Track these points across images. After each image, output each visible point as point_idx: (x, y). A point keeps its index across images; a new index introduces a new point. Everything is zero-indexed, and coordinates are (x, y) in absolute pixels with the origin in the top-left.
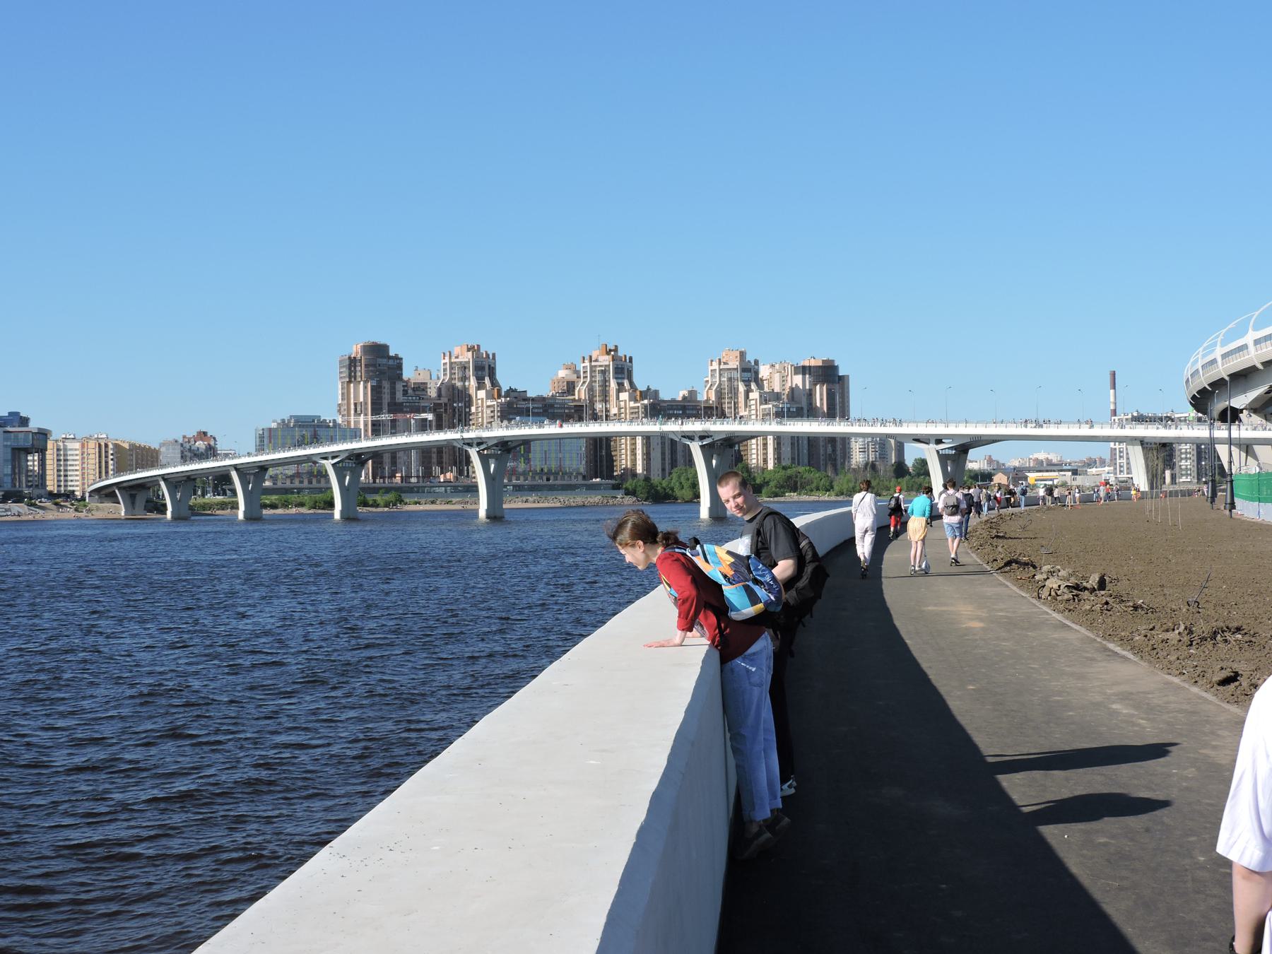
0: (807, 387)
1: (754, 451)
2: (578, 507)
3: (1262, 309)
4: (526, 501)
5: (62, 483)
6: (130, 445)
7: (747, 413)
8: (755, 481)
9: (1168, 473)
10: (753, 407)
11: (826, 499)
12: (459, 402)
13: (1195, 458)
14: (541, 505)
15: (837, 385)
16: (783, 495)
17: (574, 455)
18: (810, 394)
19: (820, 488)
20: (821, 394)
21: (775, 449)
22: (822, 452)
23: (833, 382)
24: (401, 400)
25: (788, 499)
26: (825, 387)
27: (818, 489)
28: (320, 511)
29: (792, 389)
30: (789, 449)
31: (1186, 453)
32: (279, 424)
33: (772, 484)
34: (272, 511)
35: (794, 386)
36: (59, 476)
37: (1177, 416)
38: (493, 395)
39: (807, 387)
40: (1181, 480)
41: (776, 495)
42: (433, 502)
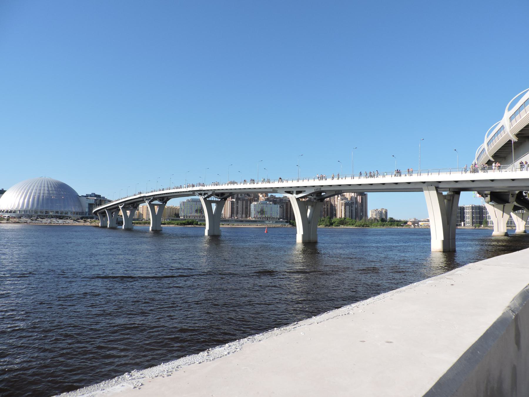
0: (355, 197)
1: (339, 214)
2: (273, 228)
3: (513, 150)
4: (257, 225)
5: (148, 217)
6: (167, 207)
7: (337, 203)
8: (331, 221)
9: (462, 223)
10: (339, 202)
11: (352, 227)
12: (256, 198)
13: (471, 219)
14: (262, 227)
15: (364, 196)
16: (339, 226)
17: (276, 212)
18: (356, 198)
19: (351, 224)
20: (359, 199)
21: (344, 213)
22: (359, 215)
23: (363, 195)
24: (240, 197)
25: (340, 227)
26: (360, 197)
27: (350, 224)
28: (179, 226)
29: (351, 197)
30: (348, 213)
31: (468, 217)
32: (187, 201)
33: (336, 223)
34: (164, 226)
35: (352, 196)
36: (147, 214)
37: (465, 206)
38: (264, 196)
39: (355, 197)
40: (467, 225)
41: (337, 226)
42: (228, 225)
